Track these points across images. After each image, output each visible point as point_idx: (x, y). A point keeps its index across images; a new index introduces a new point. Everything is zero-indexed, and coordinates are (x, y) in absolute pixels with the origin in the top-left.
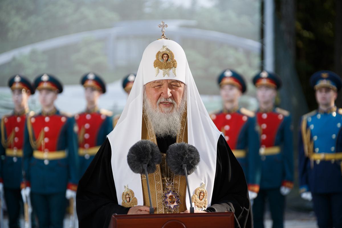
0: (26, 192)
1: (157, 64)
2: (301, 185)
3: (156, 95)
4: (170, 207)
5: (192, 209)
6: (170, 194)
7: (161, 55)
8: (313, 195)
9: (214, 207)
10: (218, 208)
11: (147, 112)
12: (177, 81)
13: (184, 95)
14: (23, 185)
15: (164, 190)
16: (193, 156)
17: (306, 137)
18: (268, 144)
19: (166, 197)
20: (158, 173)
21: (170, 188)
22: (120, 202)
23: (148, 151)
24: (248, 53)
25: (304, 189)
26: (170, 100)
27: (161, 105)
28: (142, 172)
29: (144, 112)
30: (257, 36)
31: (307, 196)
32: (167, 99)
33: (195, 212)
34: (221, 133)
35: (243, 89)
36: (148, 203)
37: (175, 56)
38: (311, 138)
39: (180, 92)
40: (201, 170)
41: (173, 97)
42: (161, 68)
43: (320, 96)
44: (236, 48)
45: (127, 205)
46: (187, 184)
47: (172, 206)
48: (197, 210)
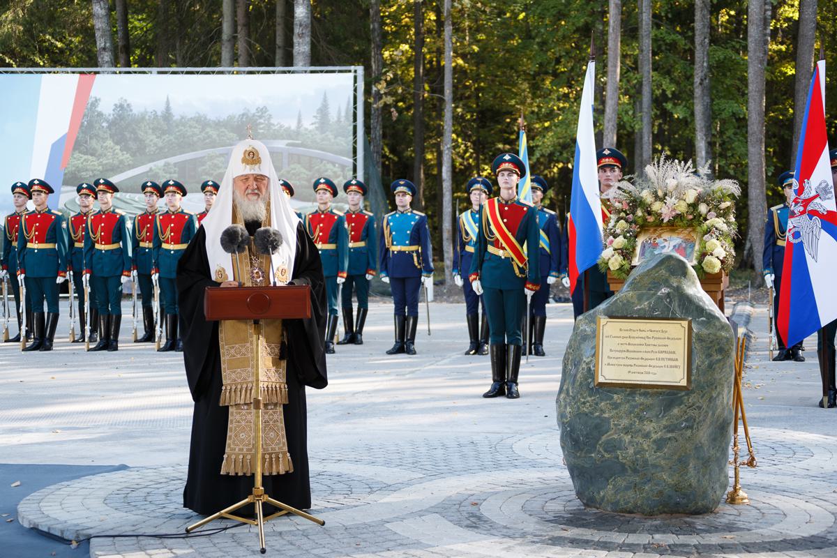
0: (155, 277)
1: (245, 161)
2: (381, 271)
3: (244, 188)
4: (256, 281)
5: (275, 283)
6: (257, 270)
7: (247, 153)
8: (391, 280)
9: (294, 281)
10: (297, 282)
11: (237, 202)
12: (262, 175)
13: (267, 187)
14: (153, 272)
15: (251, 267)
16: (276, 238)
17: (386, 232)
18: (355, 239)
19: (252, 272)
20: (247, 252)
21: (256, 265)
22: (214, 278)
23: (238, 234)
24: (343, 167)
25: (383, 275)
26: (256, 191)
27: (249, 196)
28: (233, 252)
29: (233, 201)
30: (352, 155)
31: (386, 280)
32: (253, 190)
33: (277, 285)
34: (300, 219)
35: (335, 193)
36: (237, 278)
37: (260, 153)
38: (391, 233)
39: (264, 184)
40: (283, 250)
41: (258, 189)
42: (248, 164)
43: (398, 199)
44: (333, 164)
45: (219, 281)
46: (271, 261)
47: (258, 280)
48: (278, 284)
